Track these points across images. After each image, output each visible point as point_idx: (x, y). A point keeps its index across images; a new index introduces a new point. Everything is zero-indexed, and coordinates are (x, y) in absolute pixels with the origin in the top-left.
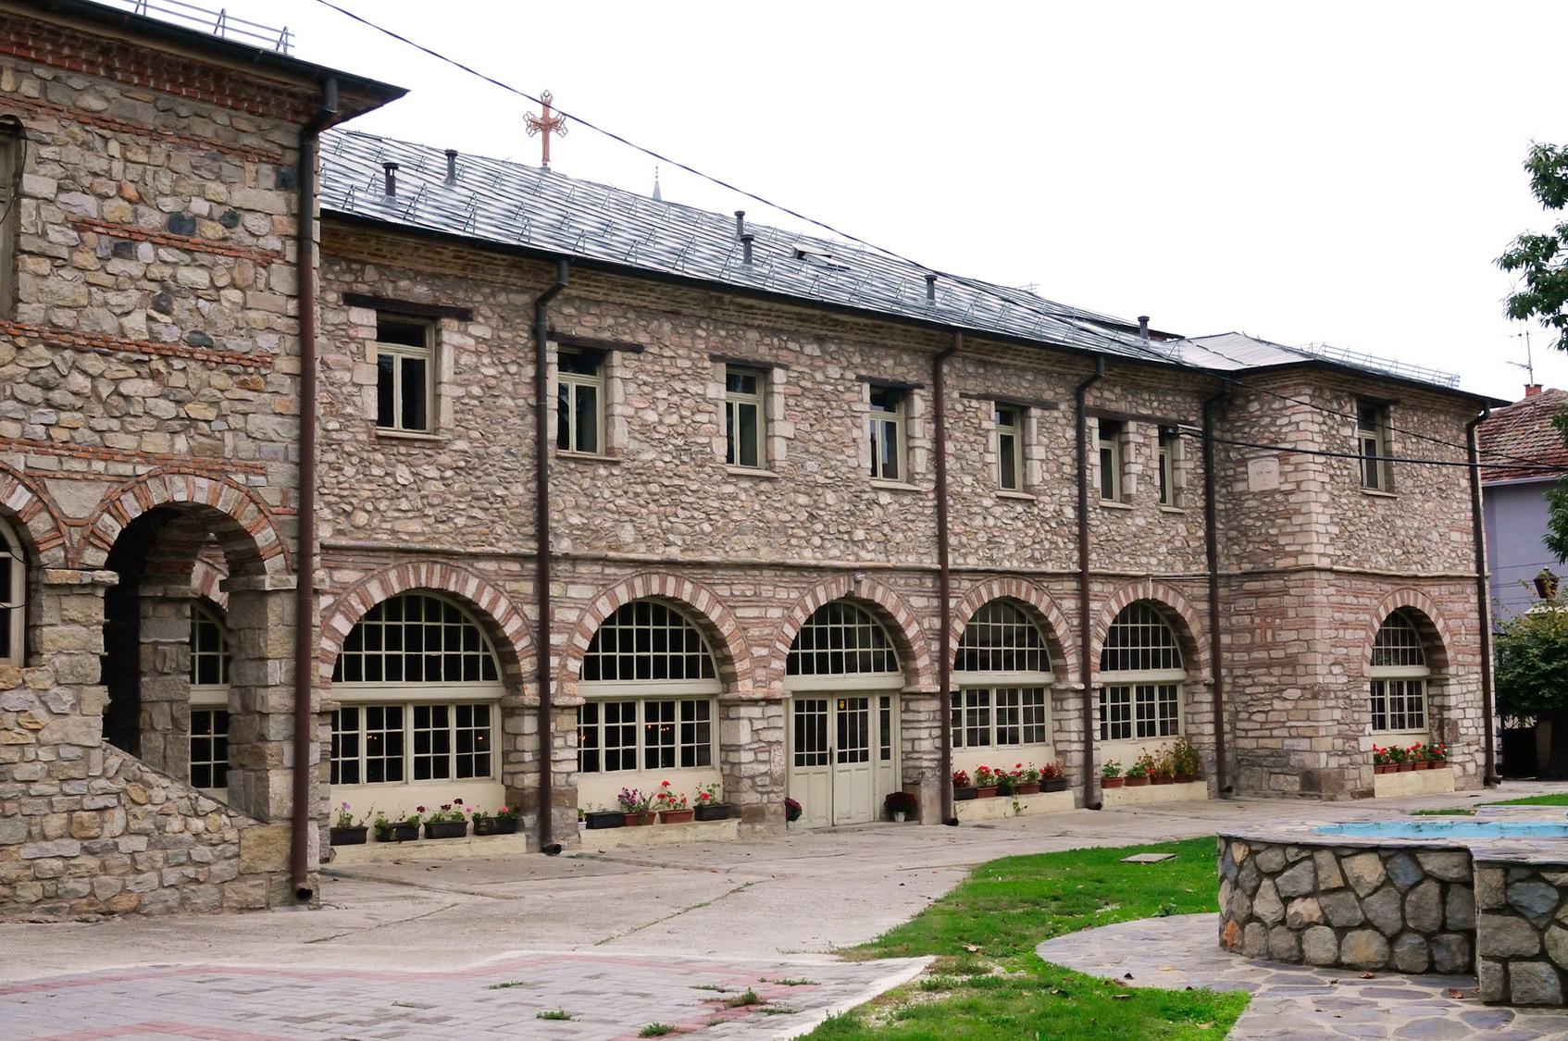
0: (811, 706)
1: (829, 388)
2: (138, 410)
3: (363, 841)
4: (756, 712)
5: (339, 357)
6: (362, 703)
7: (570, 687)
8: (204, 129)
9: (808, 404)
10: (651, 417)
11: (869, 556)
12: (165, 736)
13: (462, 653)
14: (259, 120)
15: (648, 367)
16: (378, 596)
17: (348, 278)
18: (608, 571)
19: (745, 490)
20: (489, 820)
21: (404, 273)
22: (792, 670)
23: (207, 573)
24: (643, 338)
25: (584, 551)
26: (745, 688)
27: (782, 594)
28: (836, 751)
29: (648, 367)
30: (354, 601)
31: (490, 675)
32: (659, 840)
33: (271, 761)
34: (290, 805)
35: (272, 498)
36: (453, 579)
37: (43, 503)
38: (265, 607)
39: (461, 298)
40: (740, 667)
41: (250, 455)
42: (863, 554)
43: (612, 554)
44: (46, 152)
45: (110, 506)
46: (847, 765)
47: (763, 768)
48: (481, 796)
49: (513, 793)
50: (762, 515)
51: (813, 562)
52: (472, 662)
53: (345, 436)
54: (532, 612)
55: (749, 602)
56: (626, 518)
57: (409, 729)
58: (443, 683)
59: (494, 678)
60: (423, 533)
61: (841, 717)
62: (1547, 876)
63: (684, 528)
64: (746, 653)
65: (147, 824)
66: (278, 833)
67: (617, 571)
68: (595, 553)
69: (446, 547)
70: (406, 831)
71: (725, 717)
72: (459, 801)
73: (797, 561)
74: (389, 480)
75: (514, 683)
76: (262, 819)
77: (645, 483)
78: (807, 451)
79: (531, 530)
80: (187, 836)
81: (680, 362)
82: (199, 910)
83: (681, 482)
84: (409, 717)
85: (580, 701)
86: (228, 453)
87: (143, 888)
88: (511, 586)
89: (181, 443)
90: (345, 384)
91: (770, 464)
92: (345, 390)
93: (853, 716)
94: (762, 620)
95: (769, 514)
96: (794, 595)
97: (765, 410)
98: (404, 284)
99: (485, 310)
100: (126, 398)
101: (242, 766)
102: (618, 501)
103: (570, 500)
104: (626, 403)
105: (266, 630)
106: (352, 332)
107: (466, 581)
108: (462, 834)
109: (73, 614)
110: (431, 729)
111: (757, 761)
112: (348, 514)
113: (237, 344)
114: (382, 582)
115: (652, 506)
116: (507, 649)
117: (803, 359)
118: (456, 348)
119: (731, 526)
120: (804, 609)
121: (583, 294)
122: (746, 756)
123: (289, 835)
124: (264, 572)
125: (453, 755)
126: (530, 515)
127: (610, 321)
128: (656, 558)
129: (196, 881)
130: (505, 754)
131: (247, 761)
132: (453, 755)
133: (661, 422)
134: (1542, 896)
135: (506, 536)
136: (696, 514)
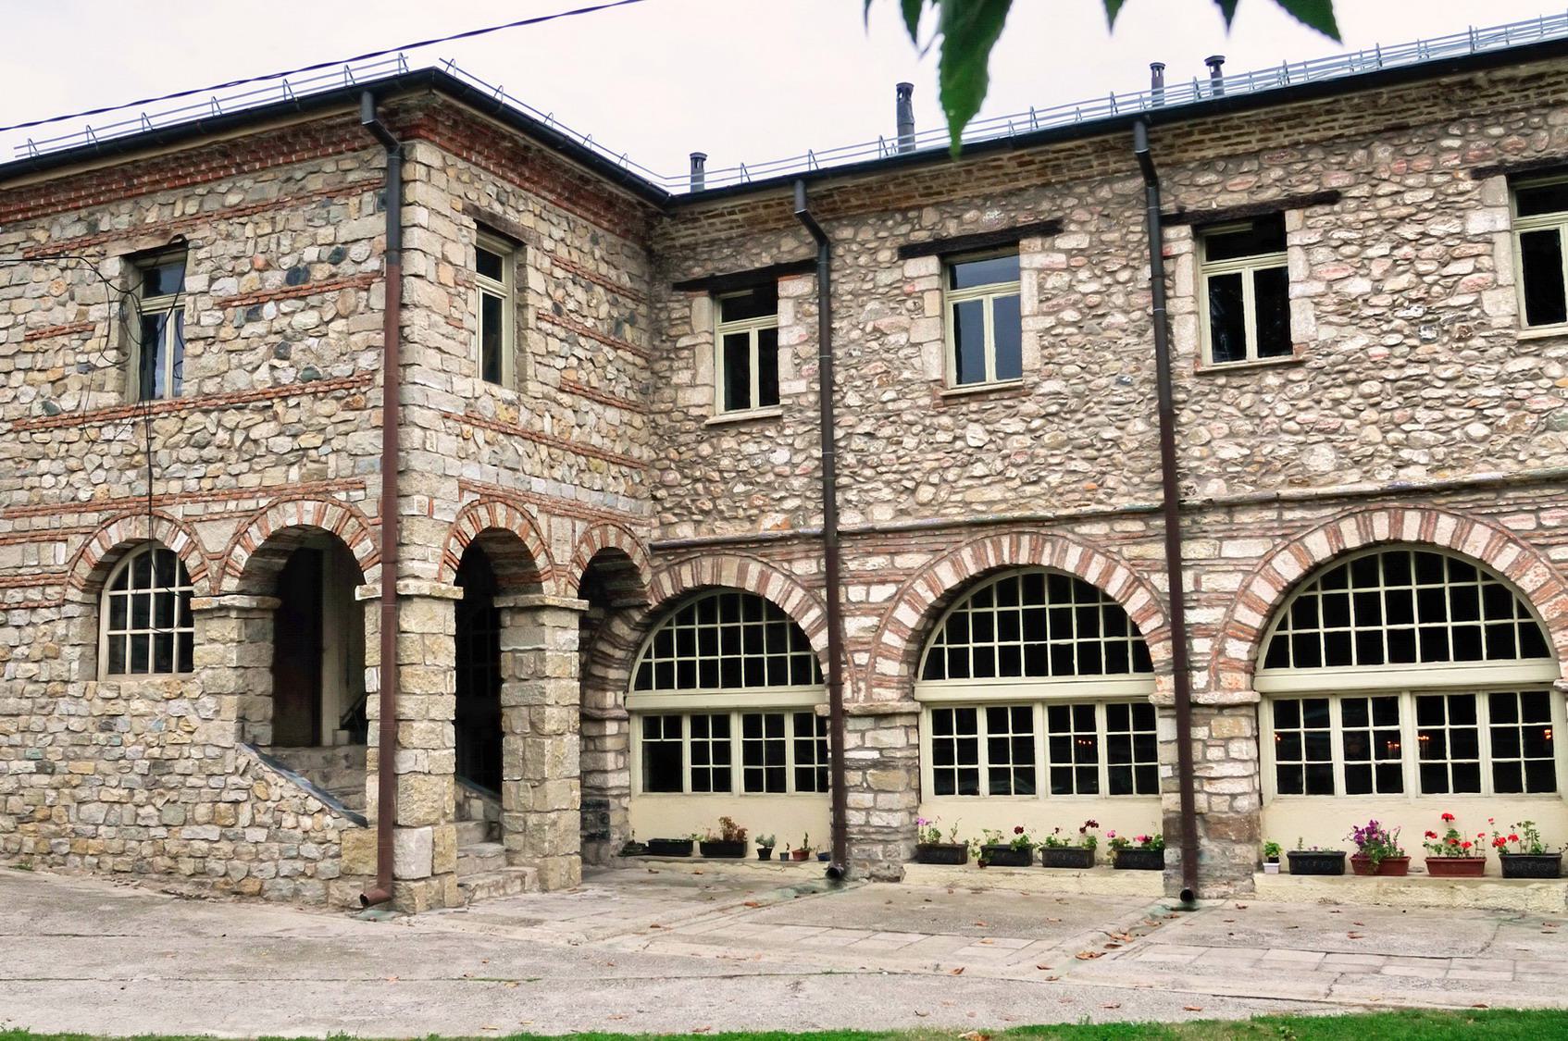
2: (262, 450)
5: (894, 319)
6: (980, 703)
8: (315, 183)
10: (1359, 286)
14: (362, 153)
15: (1349, 218)
17: (904, 229)
18: (1288, 515)
21: (969, 204)
23: (762, 573)
24: (1336, 181)
25: (1247, 491)
29: (1349, 218)
30: (920, 587)
37: (194, 545)
39: (1047, 209)
44: (201, 254)
45: (238, 537)
53: (903, 404)
54: (1161, 581)
58: (1077, 677)
60: (1005, 500)
63: (1429, 437)
65: (267, 819)
67: (1308, 514)
70: (1079, 858)
79: (1158, 475)
80: (298, 832)
83: (1425, 369)
86: (331, 475)
87: (265, 875)
89: (294, 473)
90: (902, 347)
92: (901, 354)
98: (970, 215)
99: (1081, 215)
100: (255, 441)
102: (1302, 417)
103: (1221, 427)
104: (1311, 277)
106: (907, 288)
109: (213, 634)
110: (1010, 735)
113: (342, 370)
114: (953, 564)
115: (1370, 414)
118: (1040, 270)
121: (1226, 151)
125: (1103, 765)
127: (1277, 173)
132: (1103, 765)
135: (1123, 489)
136: (1452, 412)
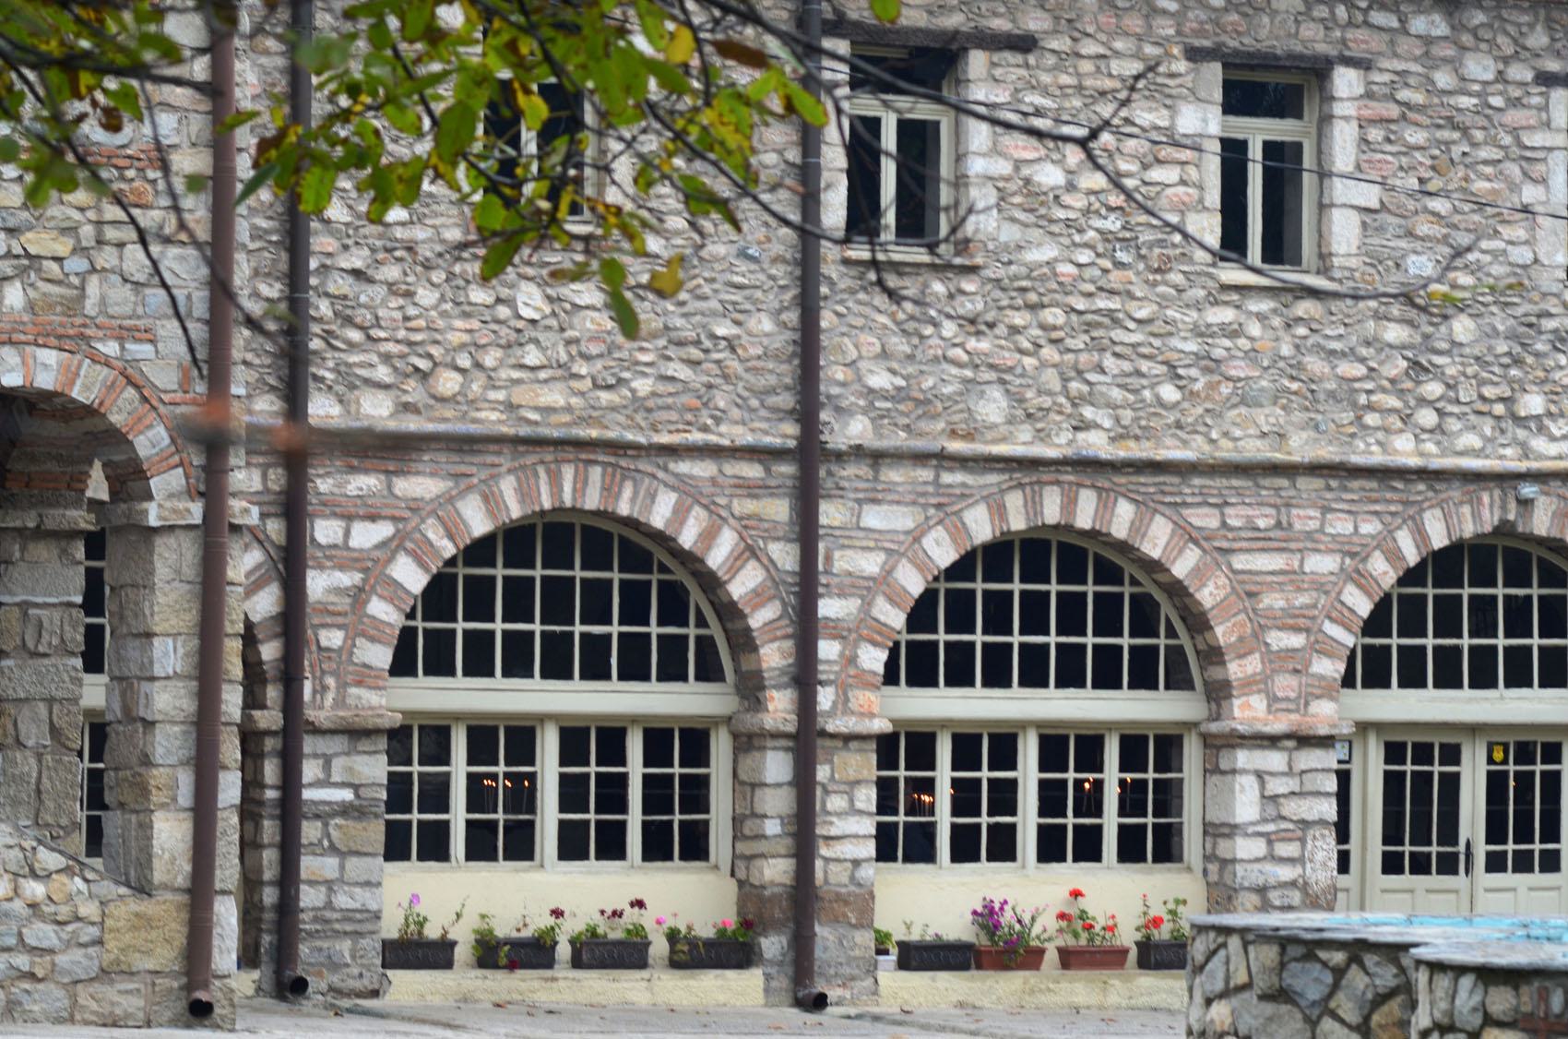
0: (1423, 753)
1: (1466, 102)
3: (447, 964)
4: (1274, 760)
7: (863, 698)
9: (1415, 136)
11: (1553, 449)
12: (39, 757)
13: (654, 629)
16: (479, 524)
18: (947, 478)
19: (1261, 317)
20: (693, 942)
22: (402, 665)
25: (900, 439)
26: (1248, 711)
27: (1341, 526)
28: (1481, 849)
29: (1046, 78)
30: (434, 533)
31: (709, 671)
32: (1043, 999)
33: (156, 797)
34: (188, 868)
35: (164, 377)
36: (627, 492)
38: (151, 553)
40: (1236, 670)
41: (128, 310)
42: (1539, 444)
43: (956, 446)
46: (1508, 878)
47: (1286, 873)
48: (684, 897)
49: (748, 892)
50: (1300, 366)
51: (1414, 462)
52: (674, 648)
53: (420, 233)
54: (785, 555)
55: (1262, 541)
56: (992, 376)
57: (548, 767)
59: (1187, 685)
60: (569, 409)
61: (1496, 783)
62: (1323, 955)
63: (1117, 394)
64: (1254, 642)
66: (167, 911)
68: (919, 444)
69: (611, 434)
71: (1212, 770)
72: (639, 904)
73: (1377, 458)
74: (503, 312)
75: (752, 689)
76: (143, 889)
77: (1032, 307)
78: (1410, 234)
79: (786, 400)
80: (18, 905)
81: (1116, 66)
82: (36, 1021)
84: (1029, 751)
85: (881, 725)
88: (749, 506)
91: (1324, 263)
93: (1525, 780)
94: (1293, 578)
95: (1315, 365)
96: (1370, 527)
97: (1320, 152)
101: (122, 805)
103: (871, 343)
105: (152, 589)
107: (652, 497)
108: (641, 963)
111: (1272, 857)
112: (424, 376)
114: (486, 499)
115: (1049, 353)
116: (738, 625)
117: (1404, 45)
119: (1226, 389)
120: (1394, 555)
122: (1246, 848)
123: (185, 916)
124: (150, 497)
126: (786, 372)
128: (1051, 453)
129: (31, 976)
130: (737, 821)
131: (127, 797)
133: (1071, 187)
134: (1317, 980)
136: (1145, 366)
